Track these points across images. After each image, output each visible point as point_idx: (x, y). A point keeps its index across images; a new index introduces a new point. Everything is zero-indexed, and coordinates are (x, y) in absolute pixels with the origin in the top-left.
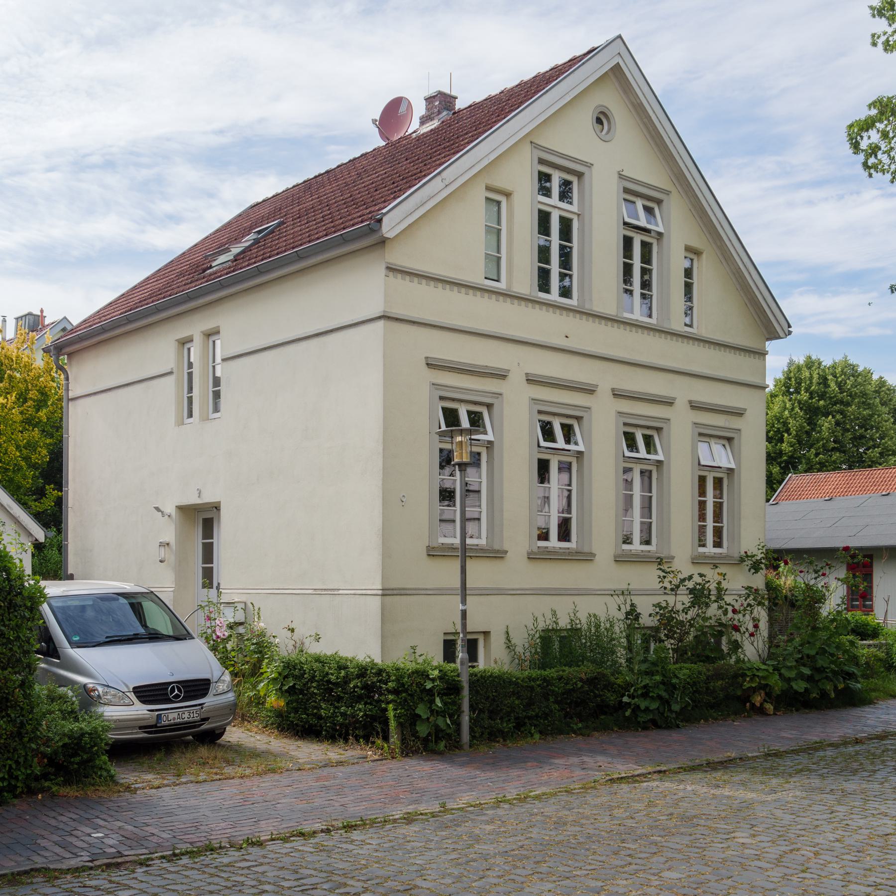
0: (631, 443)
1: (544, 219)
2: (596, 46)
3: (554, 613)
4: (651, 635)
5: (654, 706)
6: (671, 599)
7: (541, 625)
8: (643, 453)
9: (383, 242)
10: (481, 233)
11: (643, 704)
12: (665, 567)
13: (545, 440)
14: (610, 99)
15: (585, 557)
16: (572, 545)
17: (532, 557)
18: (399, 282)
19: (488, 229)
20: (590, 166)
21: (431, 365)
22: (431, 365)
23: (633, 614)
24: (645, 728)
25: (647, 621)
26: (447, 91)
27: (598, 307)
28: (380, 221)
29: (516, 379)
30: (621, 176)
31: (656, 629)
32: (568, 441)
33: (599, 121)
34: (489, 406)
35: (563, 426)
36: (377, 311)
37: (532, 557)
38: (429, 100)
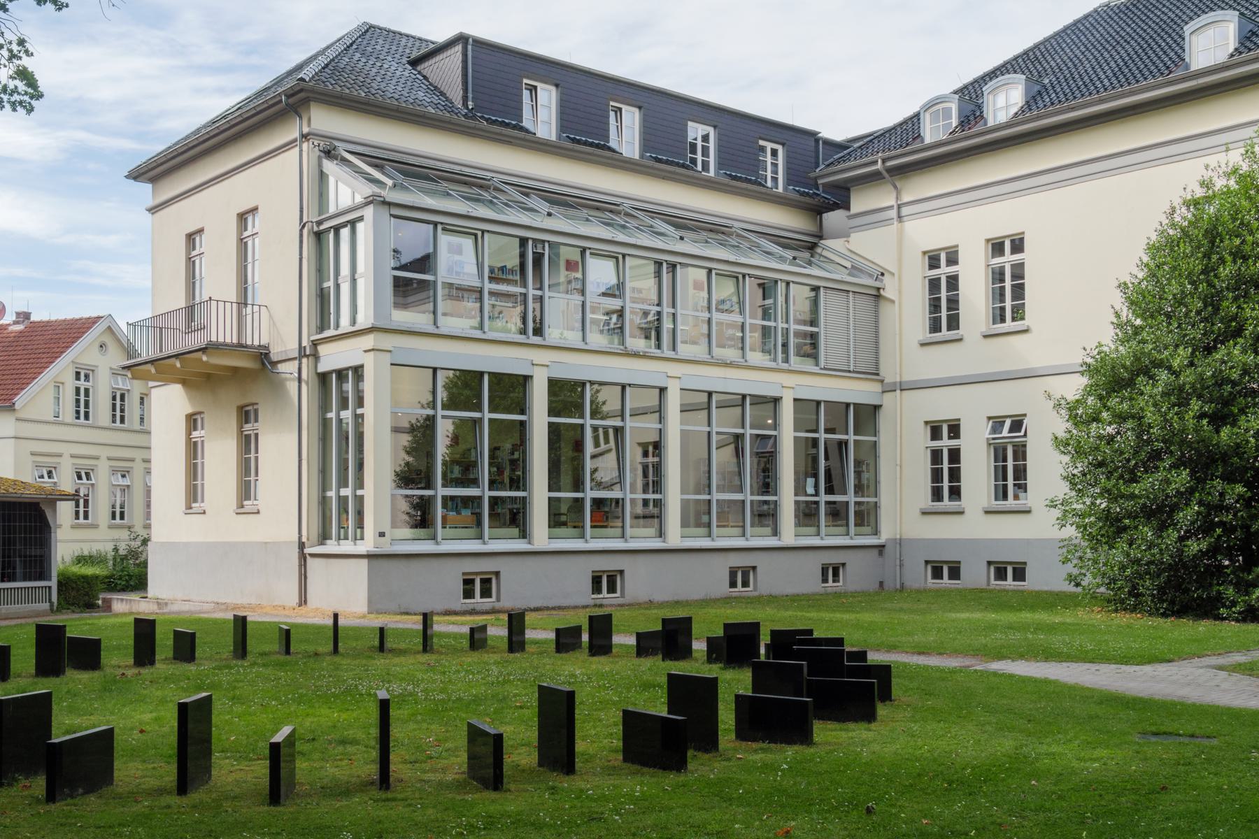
0: (80, 478)
1: (78, 389)
2: (101, 315)
3: (82, 549)
4: (124, 558)
5: (124, 583)
6: (133, 543)
7: (76, 554)
8: (85, 480)
9: (14, 410)
10: (52, 400)
11: (119, 582)
12: (132, 530)
13: (1020, 432)
14: (107, 339)
15: (95, 526)
16: (89, 521)
17: (73, 527)
18: (20, 423)
19: (55, 397)
20: (97, 367)
21: (33, 454)
22: (33, 454)
23: (116, 549)
24: (119, 591)
25: (122, 552)
26: (26, 310)
27: (101, 424)
28: (14, 404)
29: (66, 457)
30: (111, 369)
31: (126, 556)
32: (88, 479)
33: (101, 346)
34: (55, 468)
35: (86, 473)
36: (12, 434)
37: (73, 527)
38: (18, 314)
